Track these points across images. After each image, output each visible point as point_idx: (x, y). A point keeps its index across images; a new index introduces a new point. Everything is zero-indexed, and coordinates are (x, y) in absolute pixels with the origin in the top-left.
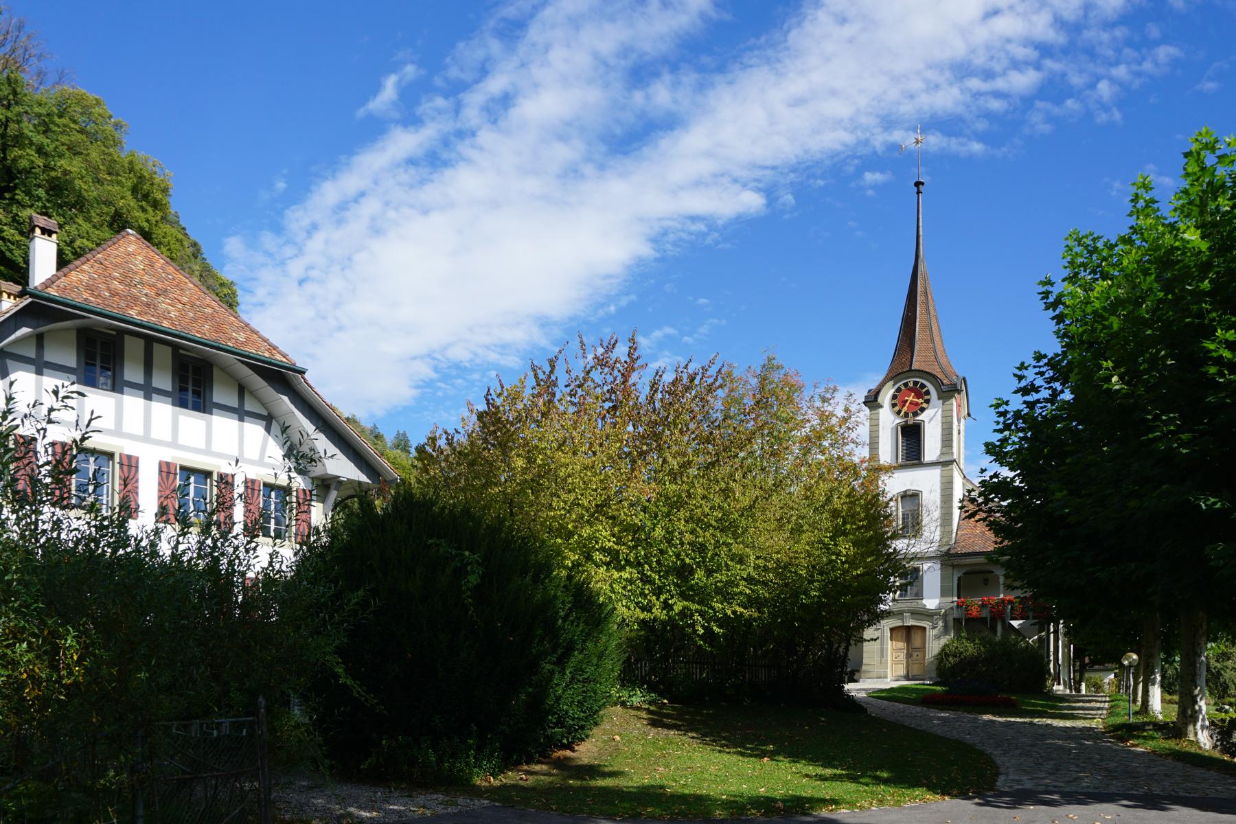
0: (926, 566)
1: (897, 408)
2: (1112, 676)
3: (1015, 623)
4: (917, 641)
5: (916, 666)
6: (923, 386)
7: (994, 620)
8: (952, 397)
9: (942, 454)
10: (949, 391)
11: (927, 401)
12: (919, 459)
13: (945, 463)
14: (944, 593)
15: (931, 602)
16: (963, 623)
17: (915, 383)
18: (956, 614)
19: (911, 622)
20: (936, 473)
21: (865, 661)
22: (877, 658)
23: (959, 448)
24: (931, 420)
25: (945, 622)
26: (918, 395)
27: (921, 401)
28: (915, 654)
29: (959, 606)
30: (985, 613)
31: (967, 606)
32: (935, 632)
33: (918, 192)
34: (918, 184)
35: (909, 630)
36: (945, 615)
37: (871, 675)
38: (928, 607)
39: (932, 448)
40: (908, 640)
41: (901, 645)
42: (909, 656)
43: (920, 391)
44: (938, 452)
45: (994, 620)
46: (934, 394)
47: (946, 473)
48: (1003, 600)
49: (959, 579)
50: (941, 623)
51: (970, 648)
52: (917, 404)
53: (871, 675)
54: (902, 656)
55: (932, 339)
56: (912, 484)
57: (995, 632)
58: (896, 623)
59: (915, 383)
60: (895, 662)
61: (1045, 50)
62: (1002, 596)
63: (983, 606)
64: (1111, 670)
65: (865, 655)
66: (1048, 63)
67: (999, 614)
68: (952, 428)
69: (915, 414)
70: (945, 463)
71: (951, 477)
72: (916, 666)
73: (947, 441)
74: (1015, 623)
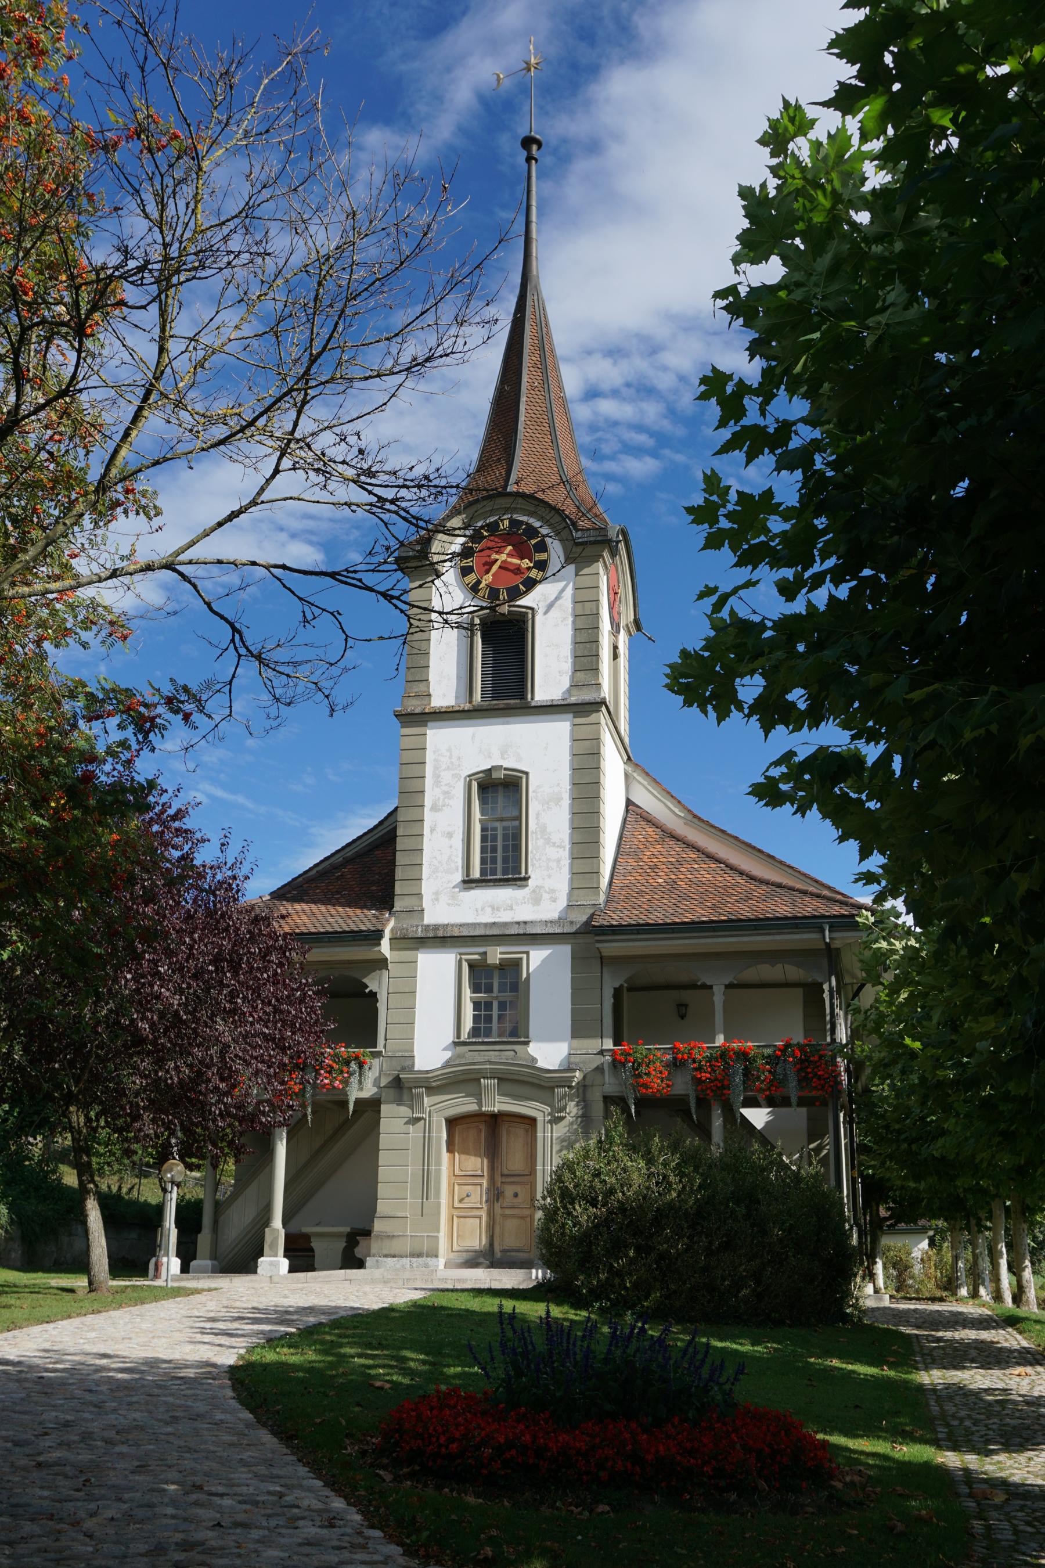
0: (537, 957)
1: (472, 578)
2: (925, 1244)
3: (758, 1117)
4: (514, 1160)
5: (511, 1224)
6: (532, 532)
7: (703, 1104)
8: (597, 558)
9: (574, 685)
10: (588, 544)
11: (542, 566)
12: (522, 696)
13: (582, 708)
14: (579, 1029)
15: (548, 1053)
16: (636, 1110)
17: (514, 523)
18: (610, 1085)
19: (498, 1104)
20: (558, 731)
21: (382, 1207)
22: (412, 1200)
23: (613, 679)
24: (551, 613)
25: (585, 1104)
26: (522, 552)
27: (526, 563)
28: (509, 1191)
29: (616, 1064)
30: (682, 1086)
31: (637, 1065)
32: (560, 1130)
33: (529, 159)
34: (528, 142)
35: (495, 1121)
36: (584, 1086)
37: (396, 1246)
38: (541, 1064)
39: (551, 673)
40: (493, 1152)
41: (475, 1164)
42: (495, 1195)
43: (524, 541)
44: (566, 683)
45: (703, 1104)
46: (556, 550)
47: (585, 732)
48: (723, 1054)
49: (617, 993)
50: (573, 1108)
51: (634, 1175)
52: (517, 570)
53: (396, 1246)
54: (477, 1196)
55: (554, 441)
56: (503, 754)
57: (706, 1134)
58: (462, 1104)
59: (514, 523)
60: (459, 1212)
61: (662, 440)
62: (720, 1040)
63: (677, 1064)
64: (924, 1230)
65: (382, 1190)
66: (667, 452)
67: (718, 1088)
68: (596, 642)
69: (515, 594)
70: (582, 708)
71: (597, 740)
72: (511, 1224)
73: (585, 657)
74: (758, 1117)
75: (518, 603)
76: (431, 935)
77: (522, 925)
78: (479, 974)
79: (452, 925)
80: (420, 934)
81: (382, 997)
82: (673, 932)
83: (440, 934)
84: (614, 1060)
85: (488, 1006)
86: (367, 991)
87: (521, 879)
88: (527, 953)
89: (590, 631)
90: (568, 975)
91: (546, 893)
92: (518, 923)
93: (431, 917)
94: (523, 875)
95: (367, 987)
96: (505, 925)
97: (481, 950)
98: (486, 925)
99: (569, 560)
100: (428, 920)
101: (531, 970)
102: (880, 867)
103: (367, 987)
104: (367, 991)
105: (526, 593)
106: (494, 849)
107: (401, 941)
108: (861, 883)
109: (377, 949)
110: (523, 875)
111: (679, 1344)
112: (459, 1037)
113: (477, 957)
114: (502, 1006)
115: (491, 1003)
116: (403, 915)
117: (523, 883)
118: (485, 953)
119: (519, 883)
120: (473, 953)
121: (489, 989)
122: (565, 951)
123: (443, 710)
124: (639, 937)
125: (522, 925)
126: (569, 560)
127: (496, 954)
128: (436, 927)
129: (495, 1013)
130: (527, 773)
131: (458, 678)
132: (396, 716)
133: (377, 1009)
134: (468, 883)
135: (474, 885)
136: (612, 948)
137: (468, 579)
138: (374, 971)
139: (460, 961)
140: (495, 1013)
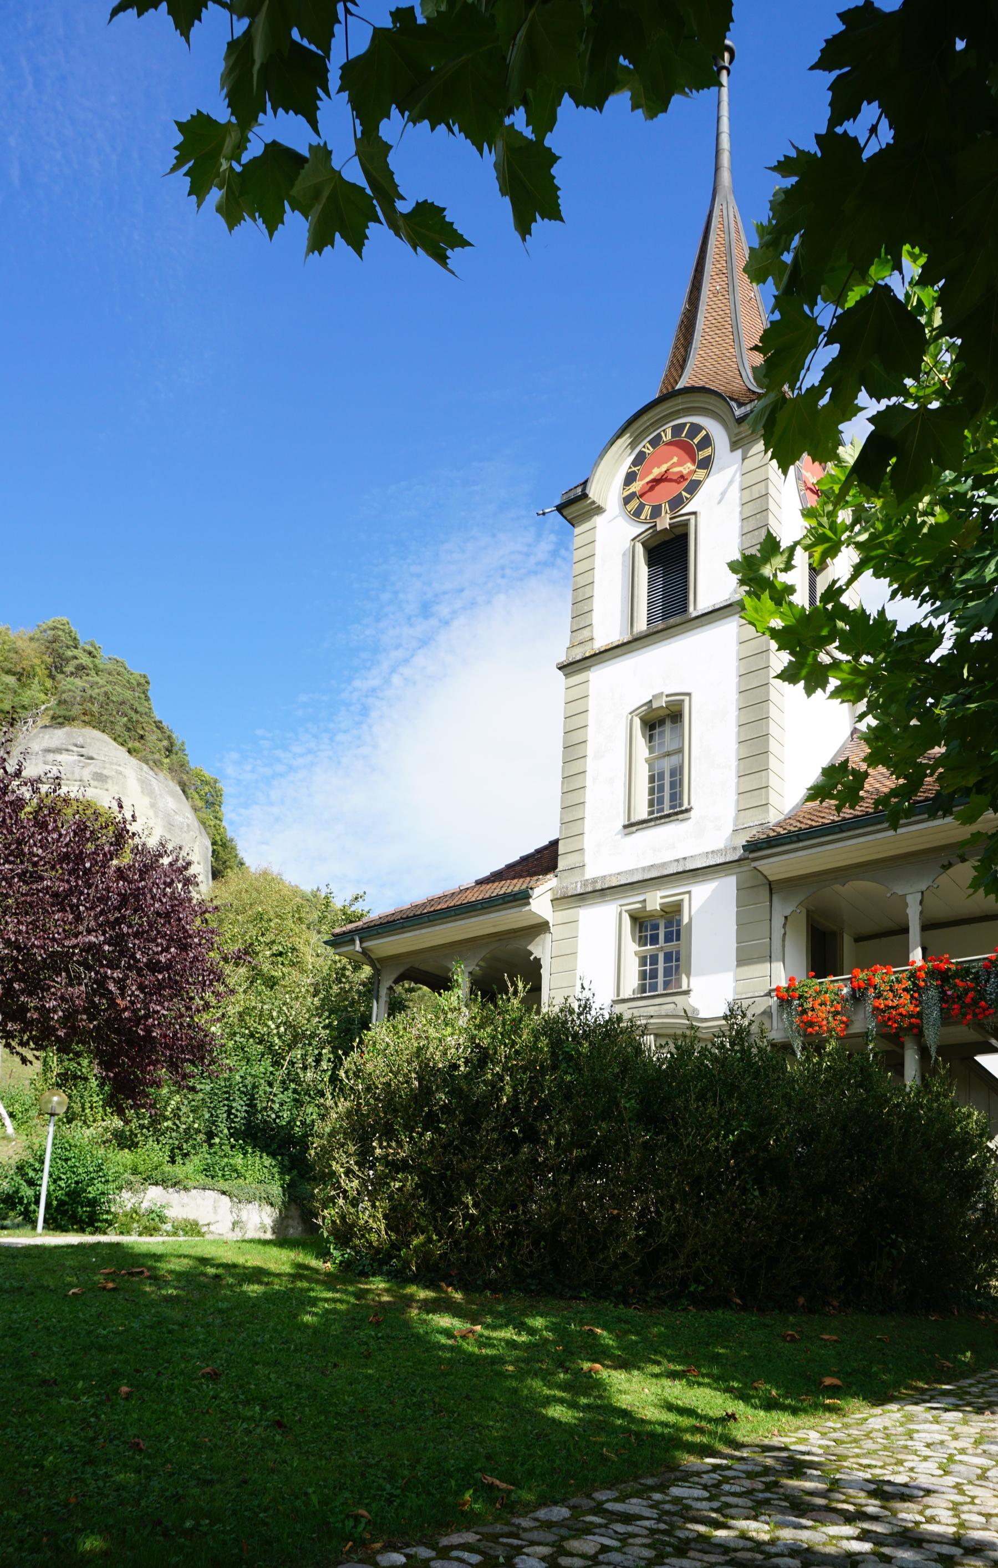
12: (685, 609)
75: (682, 512)
76: (590, 889)
77: (681, 862)
78: (644, 925)
79: (610, 875)
80: (579, 891)
81: (545, 963)
82: (842, 831)
83: (599, 887)
84: (781, 999)
85: (654, 960)
86: (532, 958)
87: (682, 812)
88: (689, 892)
89: (758, 516)
90: (733, 909)
91: (713, 823)
92: (677, 861)
93: (591, 872)
94: (686, 806)
95: (532, 954)
96: (664, 865)
97: (641, 898)
98: (644, 869)
99: (734, 445)
100: (590, 874)
101: (693, 913)
102: (785, 472)
103: (532, 954)
104: (532, 958)
105: (689, 500)
106: (661, 789)
107: (561, 900)
108: (899, 596)
109: (527, 908)
110: (686, 806)
111: (489, 1320)
112: (618, 995)
113: (639, 906)
114: (668, 957)
115: (657, 955)
116: (565, 874)
117: (685, 815)
118: (645, 901)
119: (680, 817)
120: (633, 901)
121: (654, 940)
122: (775, 898)
123: (602, 649)
124: (801, 844)
125: (681, 862)
126: (734, 445)
127: (655, 900)
128: (594, 881)
129: (661, 966)
130: (689, 694)
131: (622, 612)
132: (560, 669)
133: (540, 975)
134: (631, 826)
135: (634, 829)
136: (777, 866)
137: (629, 507)
138: (539, 935)
139: (620, 914)
140: (661, 966)
